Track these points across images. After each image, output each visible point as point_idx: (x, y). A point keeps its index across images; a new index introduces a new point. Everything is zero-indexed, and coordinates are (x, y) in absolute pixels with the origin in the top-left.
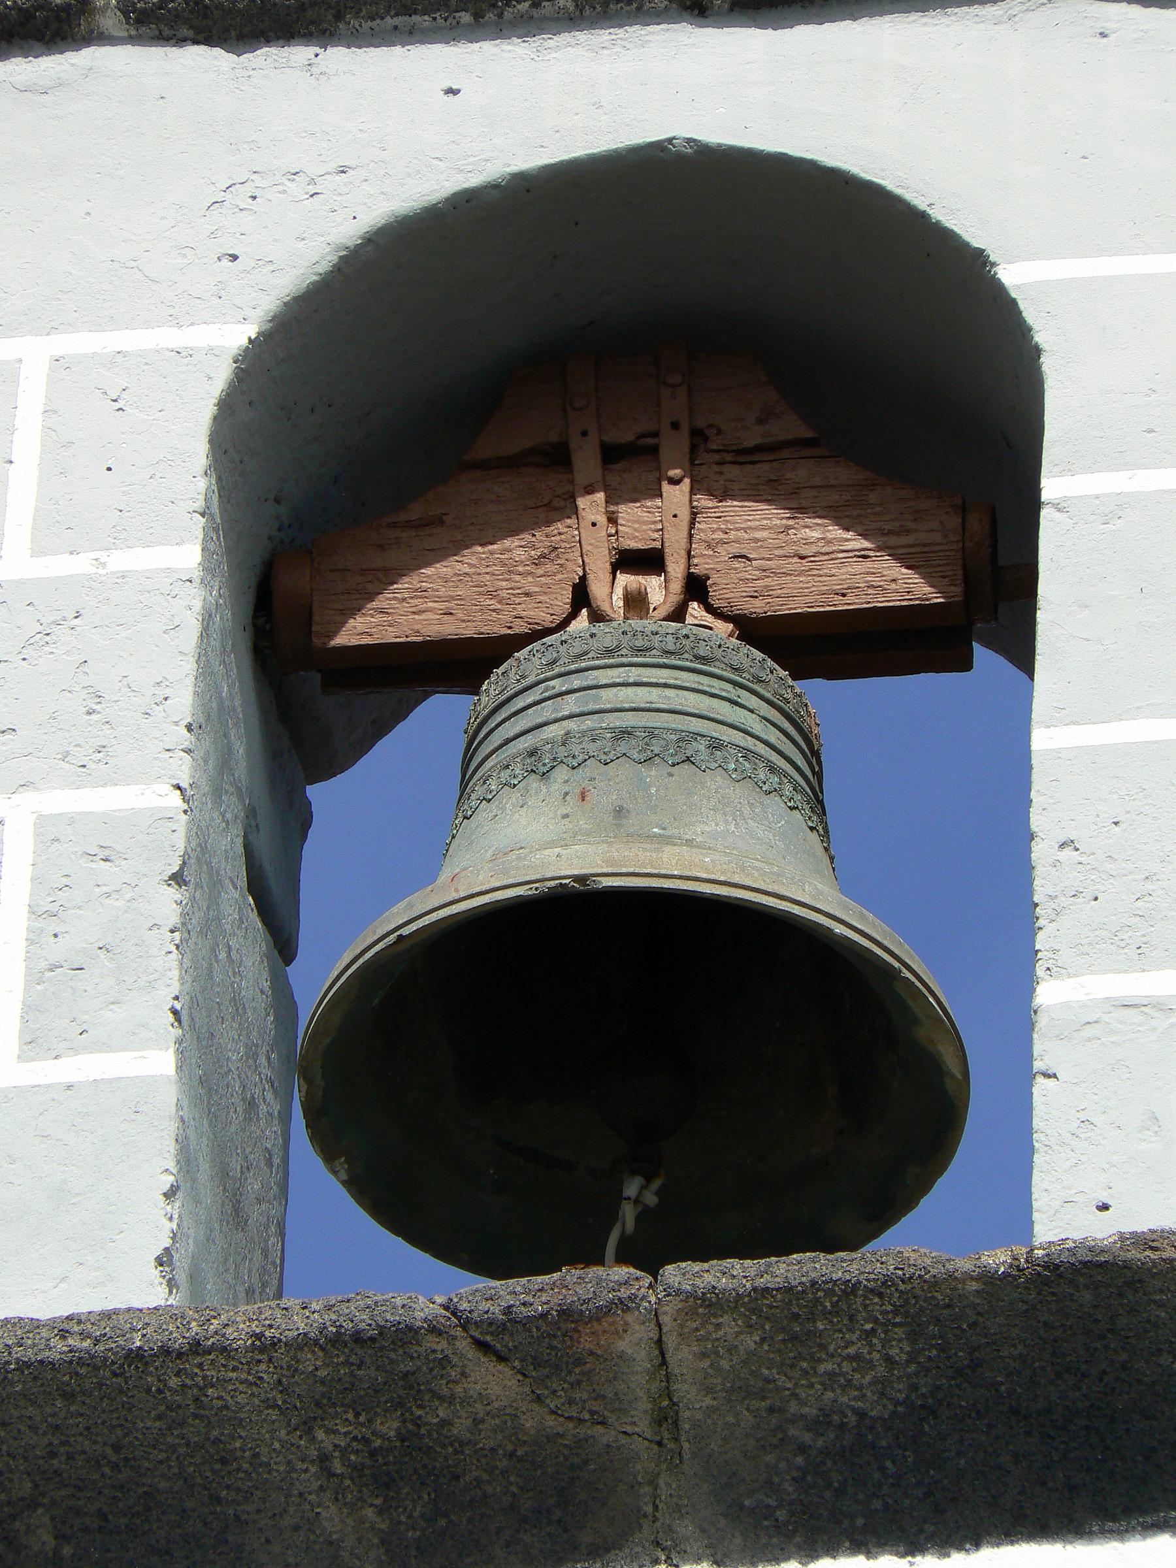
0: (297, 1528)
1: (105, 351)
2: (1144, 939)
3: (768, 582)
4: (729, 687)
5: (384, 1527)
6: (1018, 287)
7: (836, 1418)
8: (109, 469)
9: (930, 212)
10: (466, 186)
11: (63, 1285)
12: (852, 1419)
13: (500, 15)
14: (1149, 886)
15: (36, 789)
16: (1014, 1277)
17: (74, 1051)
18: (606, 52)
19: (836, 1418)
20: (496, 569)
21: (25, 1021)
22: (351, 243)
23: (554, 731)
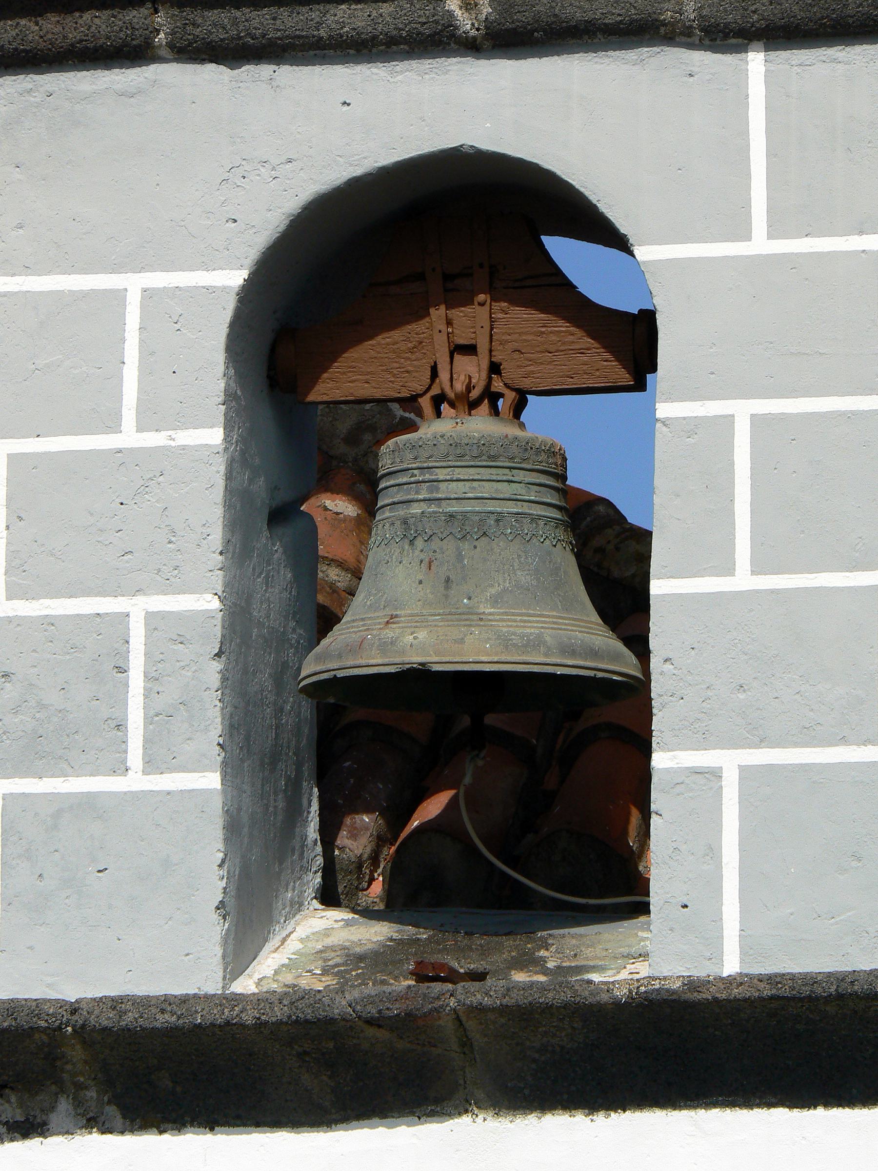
0: (290, 1083)
1: (170, 286)
2: (706, 728)
3: (531, 368)
4: (507, 471)
5: (332, 1084)
6: (644, 262)
7: (550, 1048)
8: (174, 372)
9: (598, 205)
10: (354, 175)
11: (170, 922)
12: (558, 1049)
13: (370, 51)
14: (709, 693)
15: (145, 594)
16: (630, 1003)
17: (171, 770)
18: (427, 76)
19: (550, 1048)
20: (390, 355)
21: (145, 748)
22: (296, 212)
23: (416, 509)
